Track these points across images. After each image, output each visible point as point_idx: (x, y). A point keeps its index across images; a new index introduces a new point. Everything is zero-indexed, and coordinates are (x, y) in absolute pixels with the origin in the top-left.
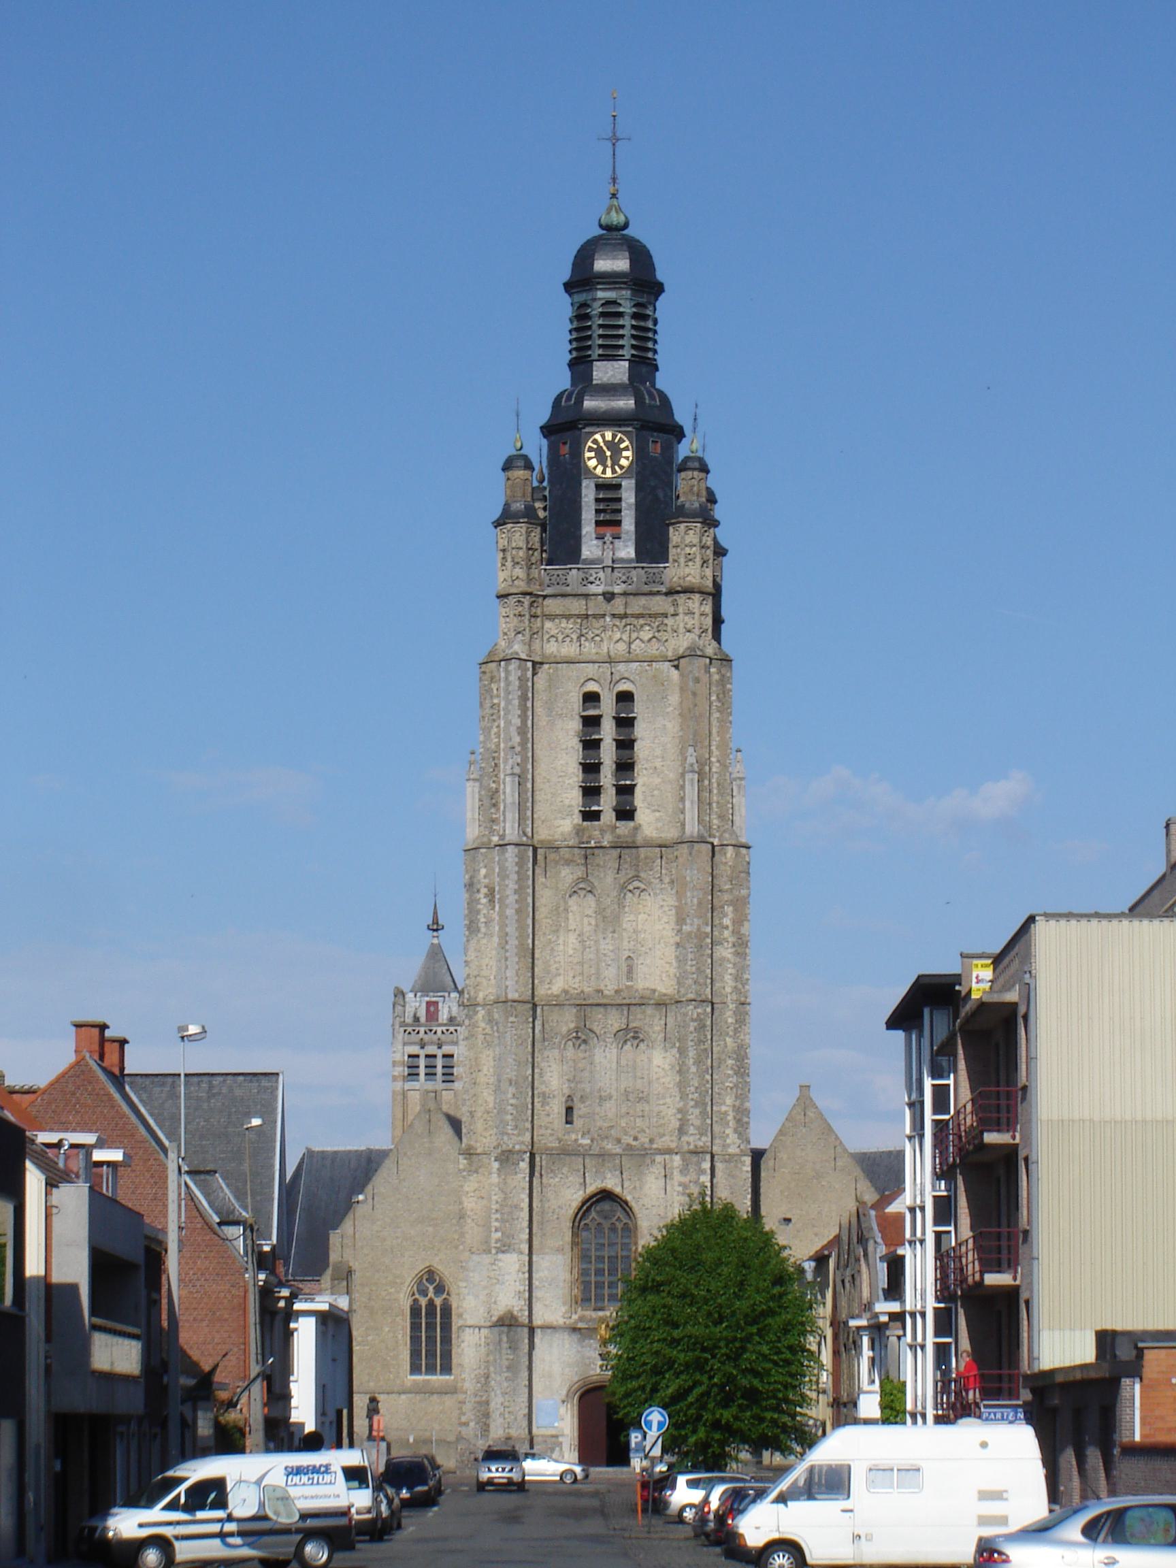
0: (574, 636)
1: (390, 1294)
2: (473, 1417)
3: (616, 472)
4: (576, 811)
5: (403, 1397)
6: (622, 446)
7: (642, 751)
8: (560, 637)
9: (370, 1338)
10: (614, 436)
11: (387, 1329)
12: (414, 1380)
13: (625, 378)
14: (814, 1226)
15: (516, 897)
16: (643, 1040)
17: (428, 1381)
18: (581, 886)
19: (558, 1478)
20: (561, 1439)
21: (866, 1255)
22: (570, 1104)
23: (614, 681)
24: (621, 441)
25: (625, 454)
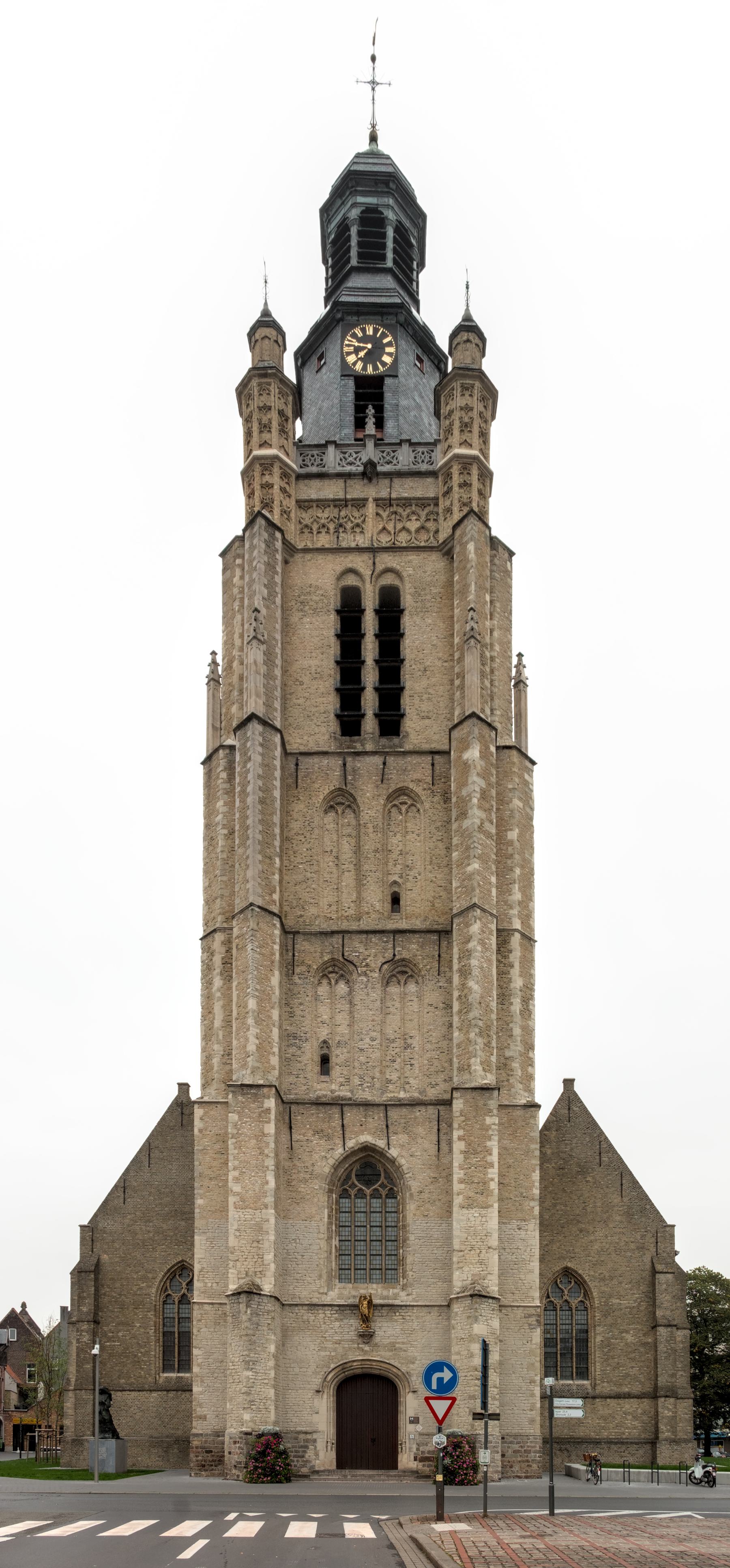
0: (332, 526)
1: (141, 1289)
2: (678, 1437)
3: (383, 332)
4: (332, 716)
5: (155, 1394)
6: (385, 341)
7: (409, 647)
8: (315, 527)
9: (120, 1334)
10: (376, 331)
11: (138, 1325)
12: (166, 1378)
13: (385, 356)
14: (579, 1222)
15: (260, 783)
16: (412, 976)
17: (182, 1377)
18: (340, 799)
19: (474, 705)
20: (315, 1436)
21: (306, 1433)
22: (325, 1051)
23: (378, 570)
24: (384, 335)
25: (388, 350)
